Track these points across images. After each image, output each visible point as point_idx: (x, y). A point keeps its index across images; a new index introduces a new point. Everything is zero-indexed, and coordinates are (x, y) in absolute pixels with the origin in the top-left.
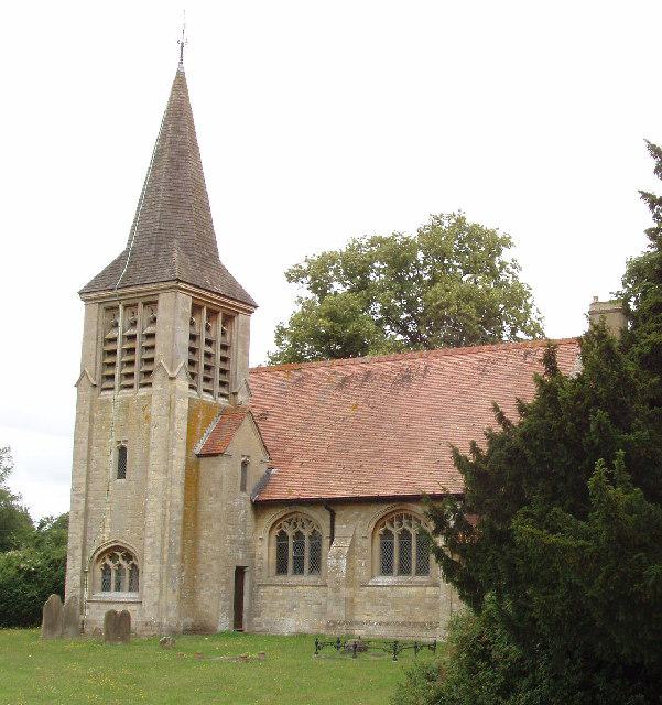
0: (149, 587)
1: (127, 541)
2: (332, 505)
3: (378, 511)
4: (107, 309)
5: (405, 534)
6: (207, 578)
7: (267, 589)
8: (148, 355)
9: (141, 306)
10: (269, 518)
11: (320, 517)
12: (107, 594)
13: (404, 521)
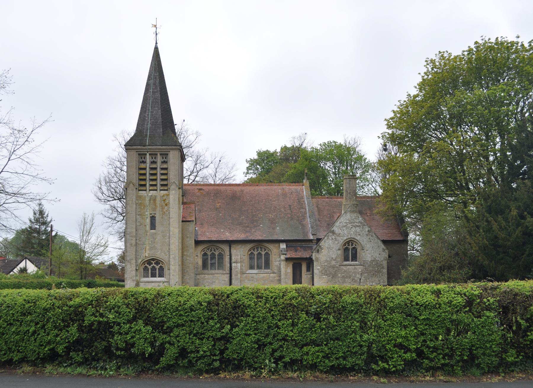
0: (173, 275)
1: (160, 255)
2: (230, 243)
3: (249, 246)
4: (139, 154)
5: (259, 254)
6: (187, 271)
7: (200, 275)
8: (164, 177)
9: (159, 155)
10: (201, 248)
11: (226, 248)
12: (348, 262)
13: (259, 249)
